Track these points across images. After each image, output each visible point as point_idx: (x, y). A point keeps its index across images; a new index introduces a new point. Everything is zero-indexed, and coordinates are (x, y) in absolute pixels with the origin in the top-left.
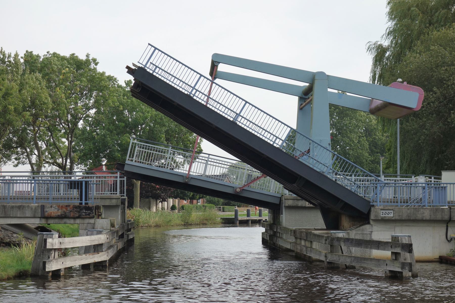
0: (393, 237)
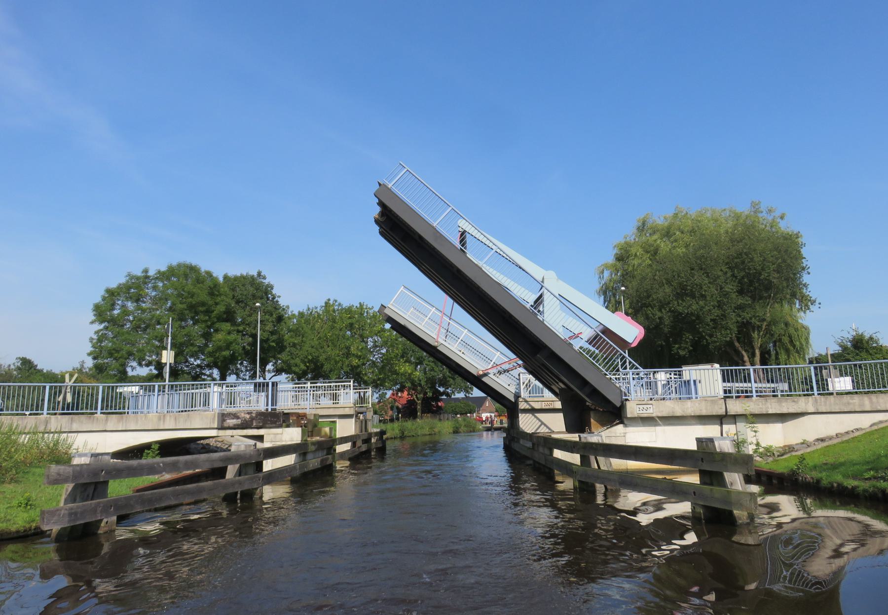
0: (699, 441)
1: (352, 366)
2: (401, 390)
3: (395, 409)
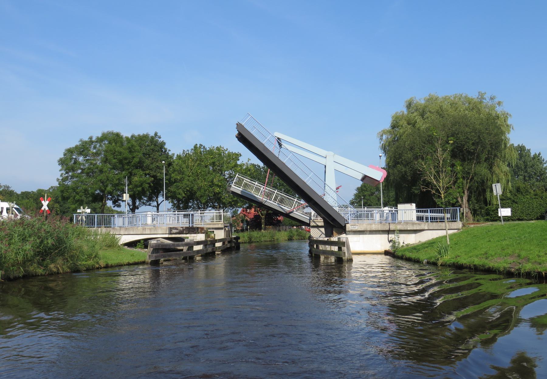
1: (214, 193)
2: (250, 207)
3: (245, 223)
